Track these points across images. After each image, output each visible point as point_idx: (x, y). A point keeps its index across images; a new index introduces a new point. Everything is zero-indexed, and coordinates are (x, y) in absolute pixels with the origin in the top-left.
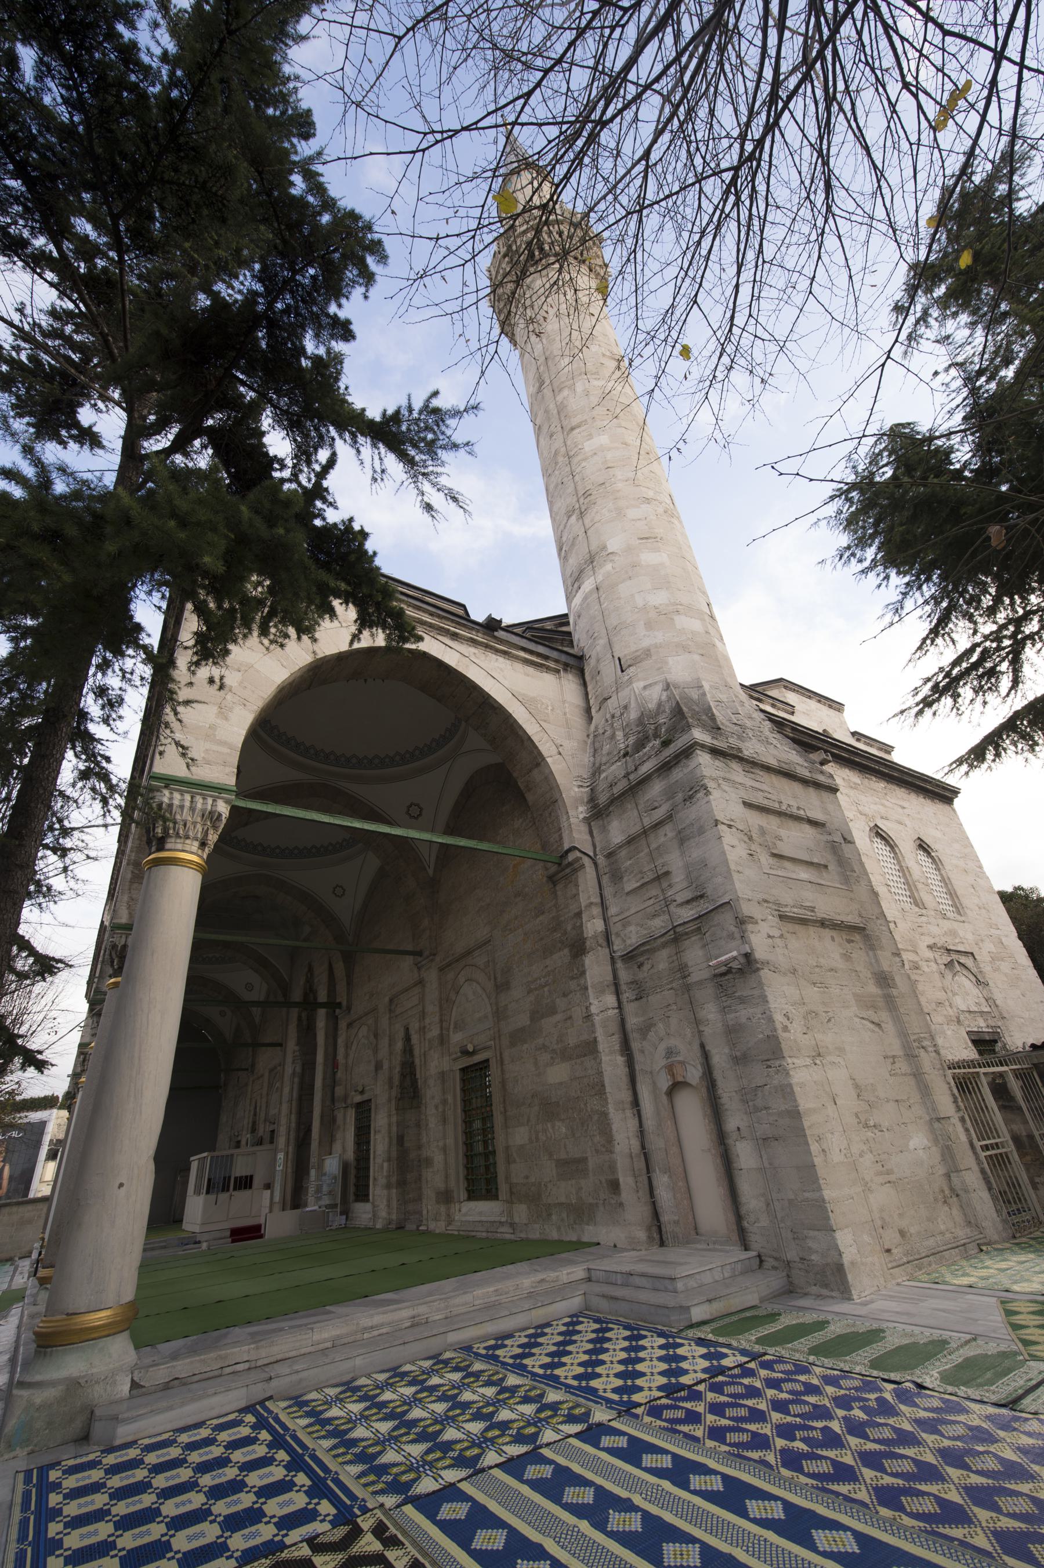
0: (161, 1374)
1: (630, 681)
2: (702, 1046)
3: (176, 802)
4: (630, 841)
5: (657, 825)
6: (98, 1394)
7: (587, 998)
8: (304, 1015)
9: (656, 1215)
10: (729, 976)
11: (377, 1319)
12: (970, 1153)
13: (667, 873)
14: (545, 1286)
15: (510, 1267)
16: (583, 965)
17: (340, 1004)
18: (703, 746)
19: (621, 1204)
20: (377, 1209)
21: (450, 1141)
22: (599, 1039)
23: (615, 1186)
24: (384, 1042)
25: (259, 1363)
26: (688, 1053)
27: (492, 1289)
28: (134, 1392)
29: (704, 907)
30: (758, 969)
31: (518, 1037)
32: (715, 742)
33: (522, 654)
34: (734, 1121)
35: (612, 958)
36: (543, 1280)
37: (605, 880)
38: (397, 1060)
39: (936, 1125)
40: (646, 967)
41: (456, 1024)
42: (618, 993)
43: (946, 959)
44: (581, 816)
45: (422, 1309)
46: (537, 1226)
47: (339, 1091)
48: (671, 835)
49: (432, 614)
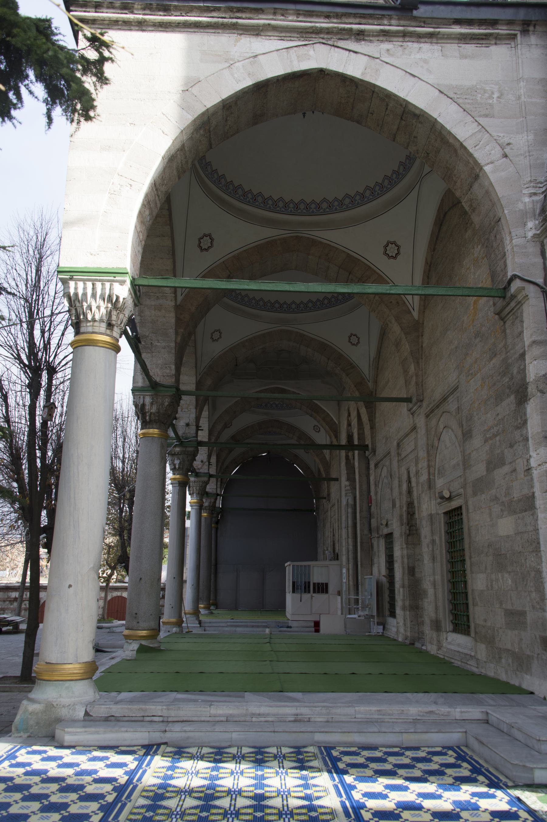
0: (101, 710)
3: (80, 292)
7: (528, 449)
14: (433, 717)
15: (421, 695)
16: (525, 414)
17: (367, 446)
21: (438, 578)
22: (536, 494)
24: (396, 483)
25: (170, 719)
28: (86, 718)
31: (480, 485)
33: (457, 29)
36: (431, 712)
38: (405, 499)
41: (439, 470)
44: (530, 234)
46: (492, 665)
47: (373, 521)
49: (328, 17)
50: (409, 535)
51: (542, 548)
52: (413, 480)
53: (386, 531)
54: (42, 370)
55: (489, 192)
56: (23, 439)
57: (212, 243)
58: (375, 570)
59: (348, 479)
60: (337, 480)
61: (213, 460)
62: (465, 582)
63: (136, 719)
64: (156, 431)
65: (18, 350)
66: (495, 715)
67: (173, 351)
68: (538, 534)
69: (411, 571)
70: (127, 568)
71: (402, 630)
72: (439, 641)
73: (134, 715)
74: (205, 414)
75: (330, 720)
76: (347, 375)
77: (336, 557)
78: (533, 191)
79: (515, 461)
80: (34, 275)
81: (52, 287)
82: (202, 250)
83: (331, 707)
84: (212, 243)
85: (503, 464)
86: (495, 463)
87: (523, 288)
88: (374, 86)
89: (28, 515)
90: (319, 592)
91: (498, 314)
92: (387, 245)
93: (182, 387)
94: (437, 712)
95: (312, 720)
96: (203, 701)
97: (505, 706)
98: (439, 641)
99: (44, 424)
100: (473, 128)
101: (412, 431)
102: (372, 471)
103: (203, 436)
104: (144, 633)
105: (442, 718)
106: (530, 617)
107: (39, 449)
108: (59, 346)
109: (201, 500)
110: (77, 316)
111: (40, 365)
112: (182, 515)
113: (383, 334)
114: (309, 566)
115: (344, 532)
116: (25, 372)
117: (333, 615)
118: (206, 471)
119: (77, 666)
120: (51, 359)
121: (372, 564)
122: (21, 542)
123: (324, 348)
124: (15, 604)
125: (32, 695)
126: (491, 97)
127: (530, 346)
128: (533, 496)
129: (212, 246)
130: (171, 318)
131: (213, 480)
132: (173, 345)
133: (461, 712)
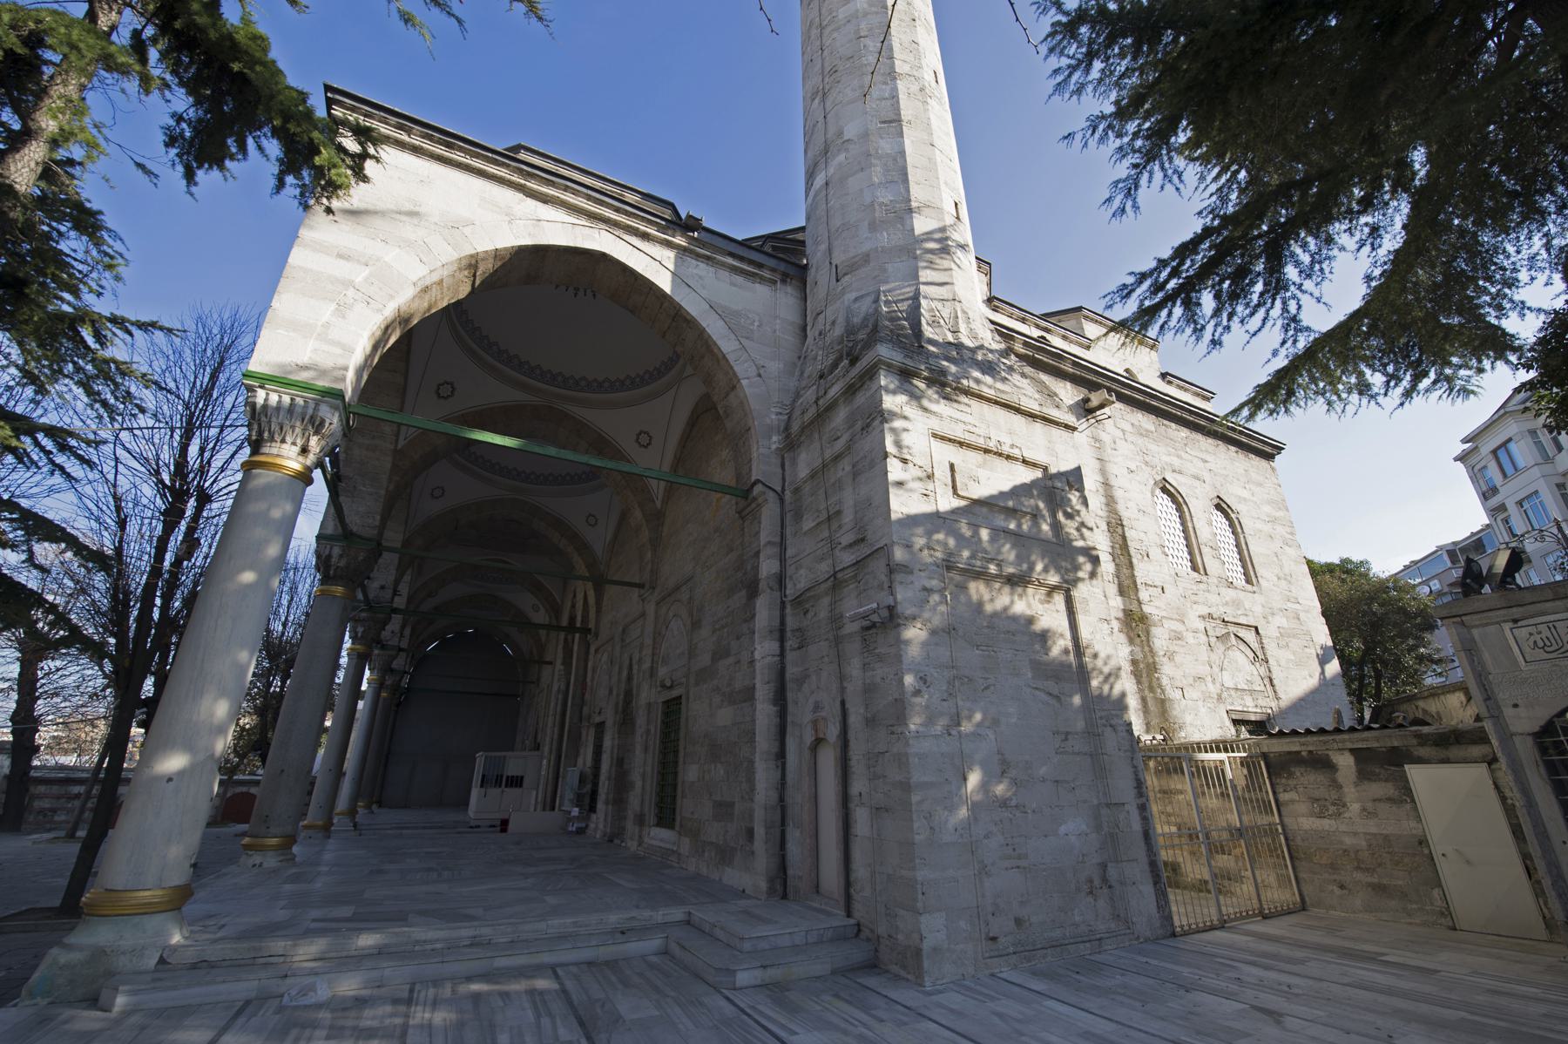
1: (843, 292)
2: (843, 703)
5: (837, 458)
9: (783, 867)
11: (431, 935)
12: (1142, 844)
13: (839, 513)
18: (889, 366)
20: (600, 821)
21: (649, 769)
23: (750, 833)
26: (832, 712)
30: (899, 625)
32: (909, 362)
33: (730, 260)
34: (858, 786)
35: (783, 603)
37: (789, 517)
39: (1104, 811)
42: (782, 640)
43: (1221, 631)
45: (486, 931)
47: (586, 710)
48: (848, 468)
52: (635, 667)
53: (598, 719)
56: (138, 581)
58: (580, 761)
61: (407, 631)
62: (676, 774)
64: (340, 589)
70: (264, 759)
74: (407, 578)
77: (537, 747)
80: (206, 380)
86: (720, 654)
93: (385, 543)
96: (349, 929)
99: (177, 563)
103: (400, 602)
104: (274, 841)
108: (222, 469)
110: (260, 433)
112: (357, 694)
113: (624, 516)
115: (550, 719)
116: (163, 496)
119: (160, 893)
124: (77, 803)
125: (71, 939)
130: (387, 463)
131: (403, 655)
132: (383, 492)
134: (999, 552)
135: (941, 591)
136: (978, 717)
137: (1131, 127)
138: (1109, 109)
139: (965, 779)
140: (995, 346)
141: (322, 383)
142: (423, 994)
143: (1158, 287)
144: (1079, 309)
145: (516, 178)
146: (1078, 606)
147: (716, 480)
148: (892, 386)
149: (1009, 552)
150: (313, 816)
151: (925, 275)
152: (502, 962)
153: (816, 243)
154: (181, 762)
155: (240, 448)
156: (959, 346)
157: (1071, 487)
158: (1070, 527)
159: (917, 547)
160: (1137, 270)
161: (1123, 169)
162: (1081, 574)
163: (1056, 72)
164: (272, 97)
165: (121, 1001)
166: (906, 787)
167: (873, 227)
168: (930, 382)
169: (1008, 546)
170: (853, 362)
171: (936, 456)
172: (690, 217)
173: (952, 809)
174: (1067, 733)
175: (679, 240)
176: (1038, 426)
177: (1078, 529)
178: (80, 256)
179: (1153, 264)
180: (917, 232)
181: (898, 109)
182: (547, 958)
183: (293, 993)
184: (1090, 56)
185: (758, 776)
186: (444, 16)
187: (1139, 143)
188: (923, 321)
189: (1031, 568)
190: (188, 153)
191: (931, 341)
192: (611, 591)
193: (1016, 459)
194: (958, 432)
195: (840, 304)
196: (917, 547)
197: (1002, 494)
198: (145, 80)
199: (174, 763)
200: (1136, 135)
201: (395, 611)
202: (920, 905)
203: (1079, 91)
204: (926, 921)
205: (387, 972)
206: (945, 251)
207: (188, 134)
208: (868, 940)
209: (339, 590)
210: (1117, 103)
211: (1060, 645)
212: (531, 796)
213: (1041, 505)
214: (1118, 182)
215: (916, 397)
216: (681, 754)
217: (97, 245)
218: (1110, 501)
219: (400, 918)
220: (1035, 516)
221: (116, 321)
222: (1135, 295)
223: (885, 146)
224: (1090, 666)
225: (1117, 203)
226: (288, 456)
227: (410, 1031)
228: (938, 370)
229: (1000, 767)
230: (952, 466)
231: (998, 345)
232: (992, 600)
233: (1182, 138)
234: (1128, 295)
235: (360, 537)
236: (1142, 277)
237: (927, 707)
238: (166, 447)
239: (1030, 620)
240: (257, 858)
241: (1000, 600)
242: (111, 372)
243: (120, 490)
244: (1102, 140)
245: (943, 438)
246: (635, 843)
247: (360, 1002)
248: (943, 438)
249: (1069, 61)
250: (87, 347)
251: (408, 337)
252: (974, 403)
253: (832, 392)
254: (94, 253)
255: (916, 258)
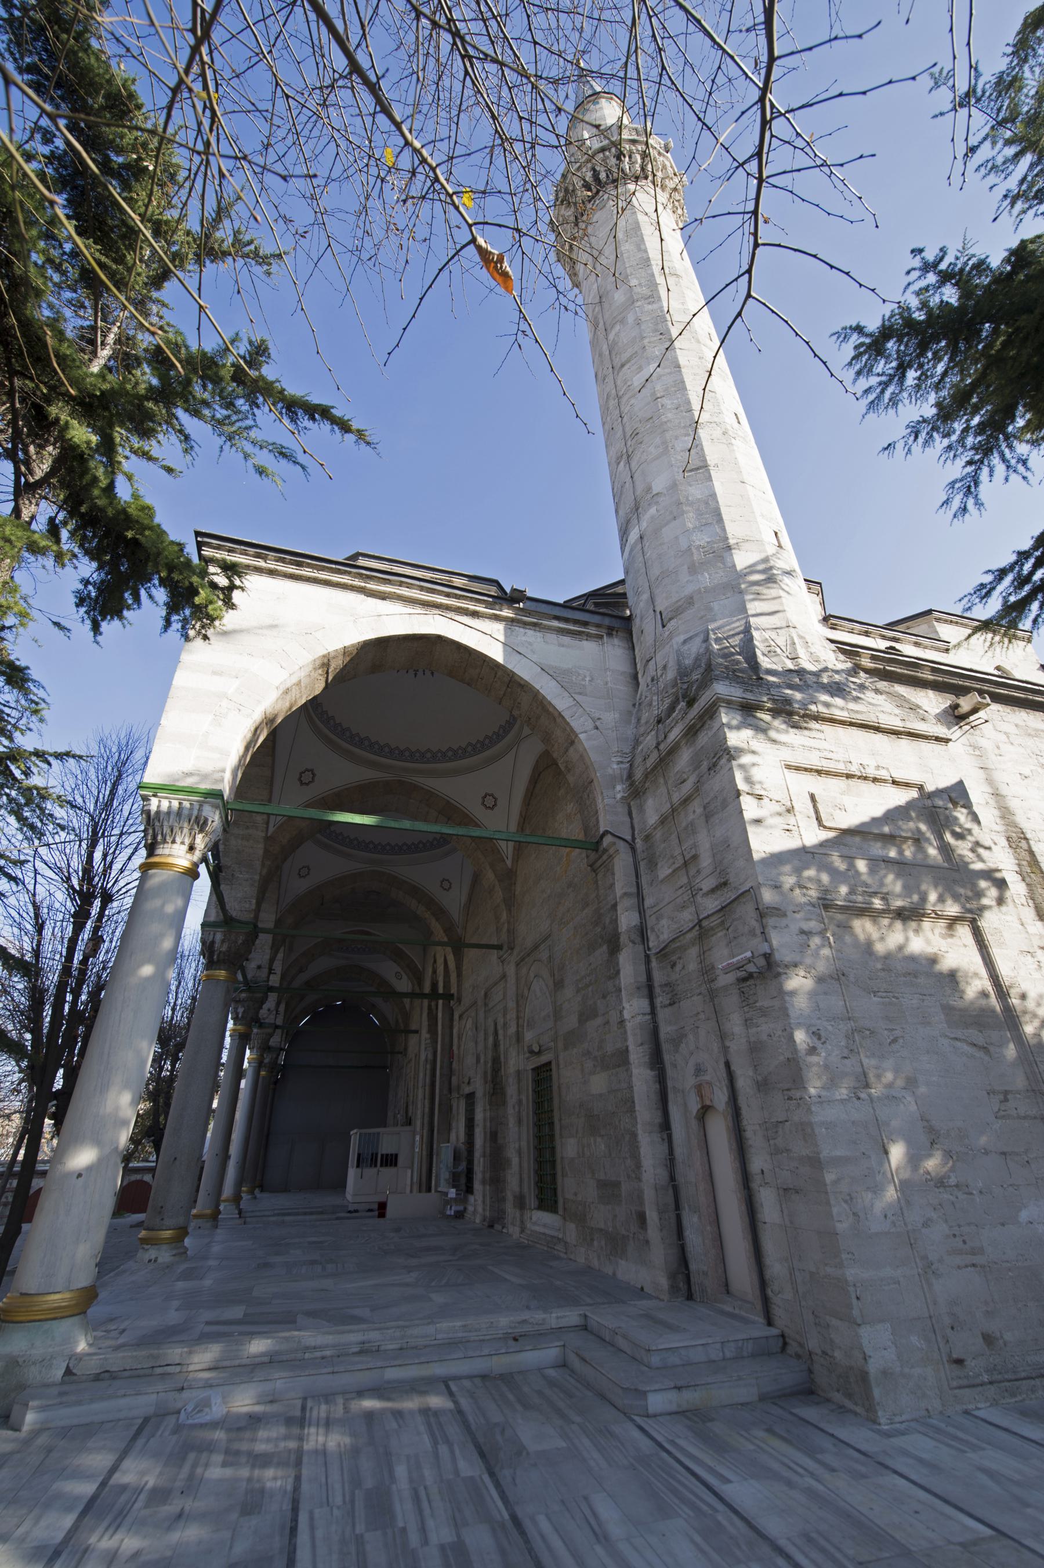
1: (671, 637)
2: (728, 1065)
4: (663, 820)
5: (686, 801)
6: (33, 1374)
8: (433, 1004)
10: (750, 982)
13: (695, 857)
16: (618, 964)
19: (647, 1242)
20: (478, 1204)
21: (524, 1144)
22: (631, 1048)
26: (715, 1074)
27: (459, 1324)
28: (66, 1378)
29: (729, 895)
30: (779, 974)
32: (749, 696)
33: (556, 624)
34: (758, 1162)
35: (647, 957)
36: (524, 1321)
37: (642, 866)
40: (678, 967)
42: (651, 997)
44: (619, 796)
45: (374, 1335)
46: (583, 1250)
47: (454, 1079)
50: (493, 1094)
51: (637, 1108)
52: (501, 1032)
53: (467, 1090)
54: (96, 898)
55: (582, 757)
56: (51, 979)
57: (313, 778)
59: (429, 1032)
60: (416, 1032)
63: (141, 1372)
65: (68, 872)
66: (596, 1318)
67: (256, 884)
68: (632, 1091)
69: (494, 1136)
70: (157, 1147)
71: (480, 1209)
72: (522, 1222)
73: (139, 1366)
74: (280, 955)
75: (405, 1346)
76: (437, 920)
77: (409, 1122)
78: (620, 759)
79: (608, 1013)
80: (107, 793)
81: (126, 808)
82: (302, 784)
83: (407, 1327)
84: (313, 778)
85: (596, 1016)
86: (587, 1014)
87: (614, 844)
88: (486, 656)
89: (37, 1075)
90: (386, 1165)
91: (591, 866)
92: (485, 797)
93: (260, 925)
94: (532, 1320)
95: (382, 1348)
96: (241, 1334)
97: (603, 1304)
98: (522, 1222)
99: (84, 962)
100: (569, 702)
101: (501, 980)
102: (456, 1023)
103: (275, 980)
104: (167, 1234)
105: (537, 1328)
106: (625, 1188)
107: (71, 992)
108: (122, 871)
109: (262, 1056)
110: (154, 837)
111: (94, 891)
113: (476, 879)
114: (378, 1134)
116: (73, 900)
117: (399, 1188)
118: (272, 1021)
120: (109, 886)
121: (450, 1130)
122: (19, 1112)
123: (416, 891)
126: (583, 680)
127: (622, 897)
128: (627, 1050)
129: (313, 781)
130: (259, 849)
131: (279, 1031)
132: (257, 877)
133: (558, 1318)
134: (882, 884)
135: (822, 933)
136: (889, 1076)
137: (958, 426)
138: (930, 412)
139: (886, 1153)
140: (840, 666)
141: (205, 786)
142: (315, 1413)
143: (1022, 581)
144: (929, 612)
145: (357, 583)
146: (990, 938)
147: (564, 835)
148: (735, 722)
149: (893, 883)
150: (202, 1206)
151: (753, 607)
152: (392, 1374)
153: (638, 594)
154: (86, 1158)
155: (136, 850)
156: (801, 672)
157: (955, 804)
158: (963, 848)
159: (787, 886)
160: (994, 567)
161: (957, 469)
162: (985, 901)
163: (867, 391)
164: (159, 554)
165: (30, 1418)
166: (815, 1162)
167: (693, 570)
168: (776, 713)
169: (890, 877)
170: (691, 703)
171: (793, 791)
172: (514, 590)
173: (877, 1189)
174: (1006, 1093)
175: (507, 613)
176: (905, 743)
177: (973, 850)
178: (13, 705)
179: (1013, 558)
180: (739, 568)
181: (704, 456)
182: (438, 1370)
183: (189, 1408)
184: (902, 369)
185: (642, 1151)
186: (291, 465)
187: (970, 441)
188: (758, 653)
189: (924, 899)
190: (94, 609)
191: (770, 672)
192: (470, 954)
193: (885, 781)
194: (814, 760)
195: (669, 649)
196: (787, 886)
197: (874, 820)
198: (59, 557)
199: (83, 1158)
200: (966, 430)
201: (271, 989)
202: (855, 1312)
203: (894, 402)
204: (865, 1333)
205: (279, 1384)
206: (771, 580)
207: (93, 594)
208: (798, 1356)
209: (222, 974)
210: (938, 405)
211: (977, 984)
212: (406, 1176)
213: (923, 827)
214: (954, 482)
215: (762, 730)
216: (557, 1127)
217: (26, 694)
218: (1006, 814)
219: (288, 1320)
220: (918, 840)
221: (39, 754)
222: (996, 594)
223: (695, 492)
224: (1018, 1009)
225: (956, 503)
226: (178, 854)
227: (305, 1459)
228: (784, 699)
229: (928, 1136)
230: (813, 797)
231: (842, 664)
232: (882, 939)
233: (1020, 423)
234: (988, 594)
235: (239, 922)
236: (1002, 573)
237: (826, 1067)
238: (75, 856)
239: (933, 960)
240: (152, 1253)
241: (892, 938)
242: (36, 797)
243: (38, 898)
244: (926, 443)
245: (798, 769)
246: (517, 1229)
247: (254, 1421)
248: (798, 769)
249: (879, 379)
250: (15, 779)
251: (273, 735)
252: (827, 728)
253: (673, 735)
254: (23, 702)
255: (741, 592)
